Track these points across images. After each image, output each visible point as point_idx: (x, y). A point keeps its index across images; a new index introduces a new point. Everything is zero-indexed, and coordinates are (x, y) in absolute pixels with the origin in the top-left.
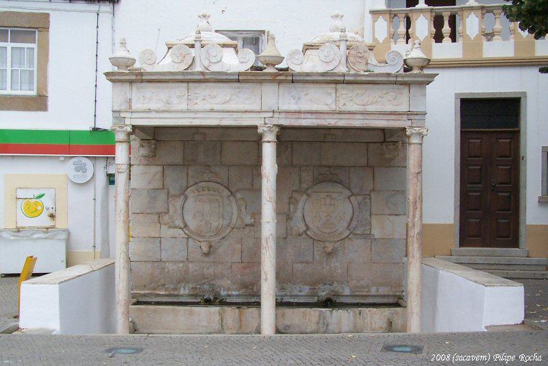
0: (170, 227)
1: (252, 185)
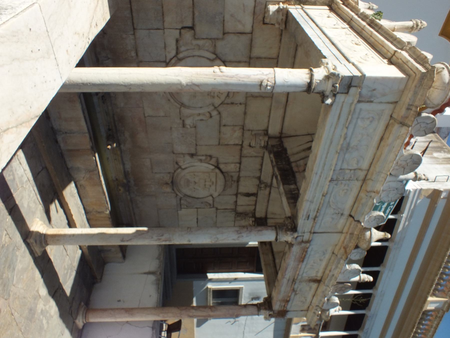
0: (177, 41)
1: (225, 126)
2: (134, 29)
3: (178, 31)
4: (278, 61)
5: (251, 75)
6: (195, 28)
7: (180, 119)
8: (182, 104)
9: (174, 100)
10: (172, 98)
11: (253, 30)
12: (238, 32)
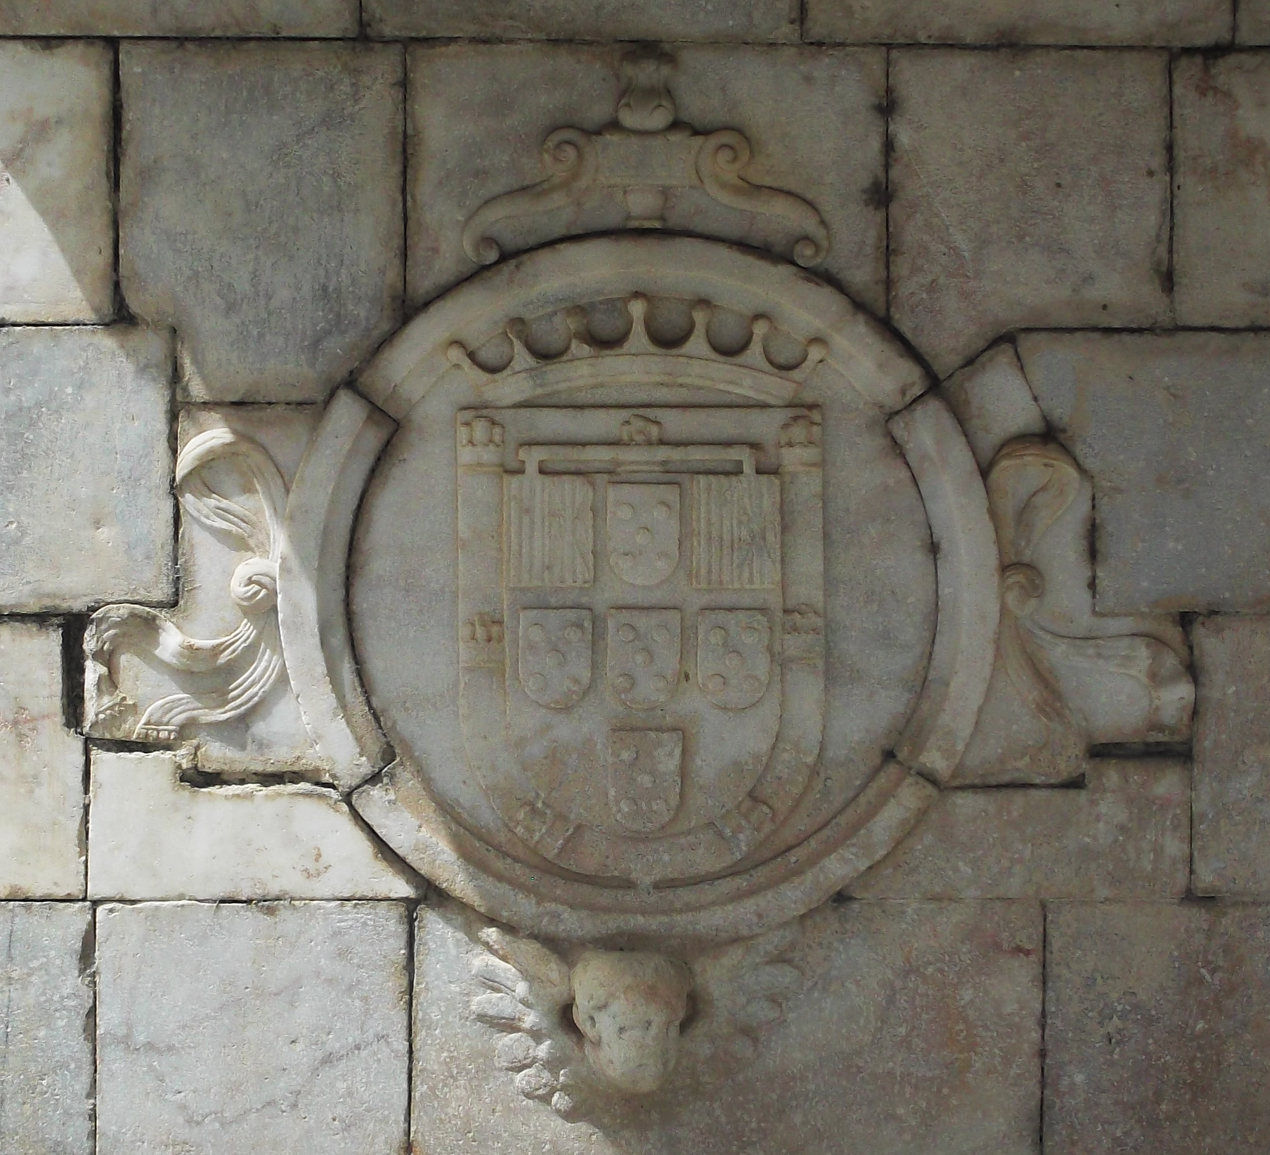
1: (1168, 280)
6: (78, 605)
7: (1075, 784)
9: (831, 847)
10: (815, 859)
11: (89, 39)
12: (104, 186)
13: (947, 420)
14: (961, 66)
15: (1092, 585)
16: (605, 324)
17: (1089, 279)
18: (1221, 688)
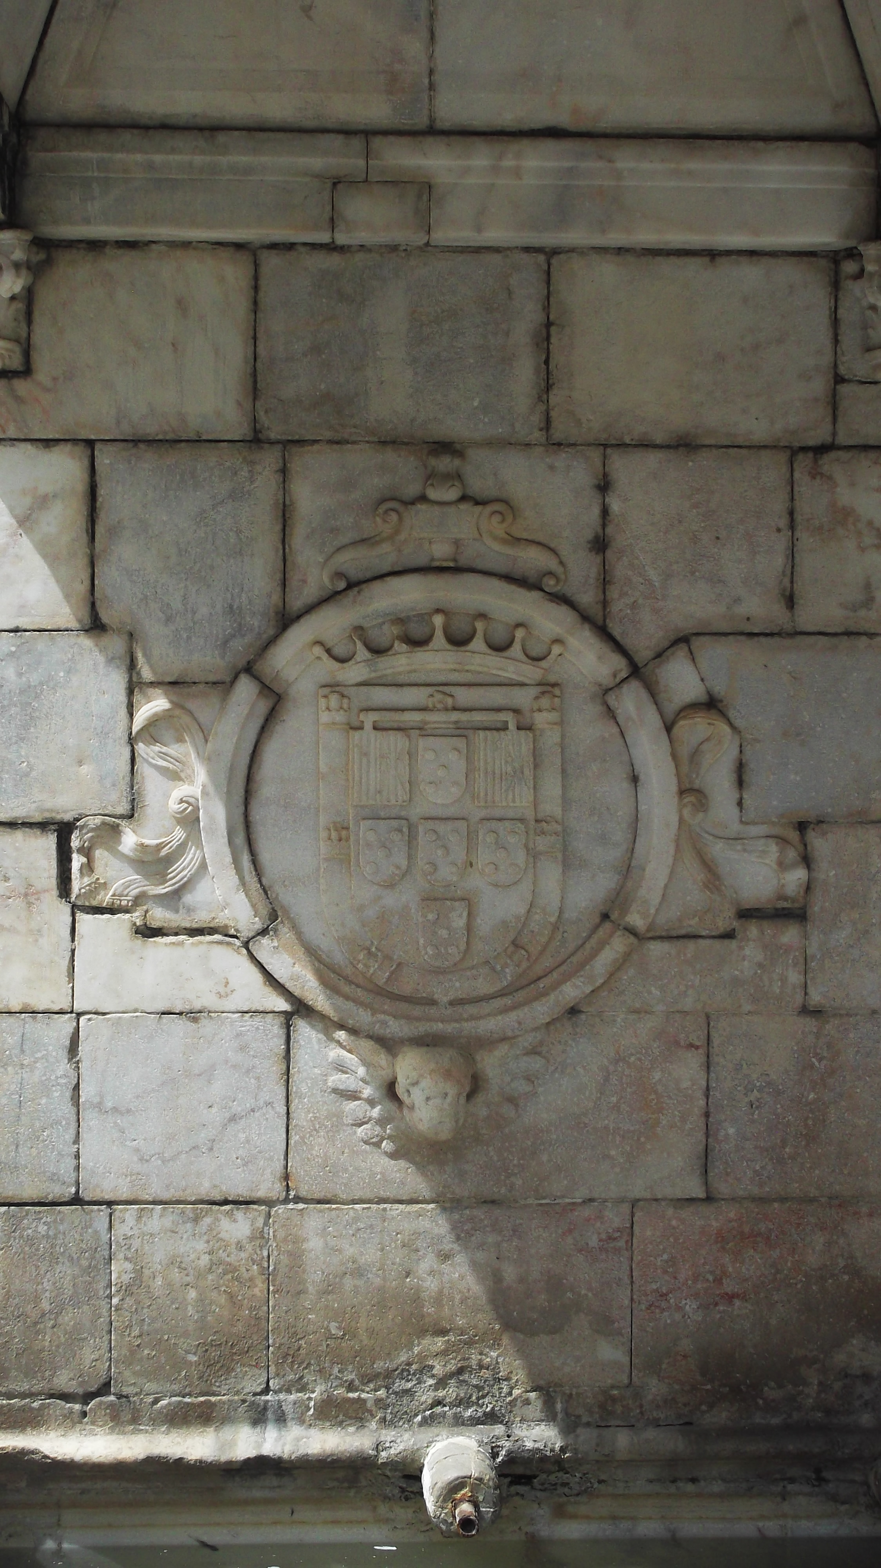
1: (790, 601)
2: (76, 1200)
3: (83, 918)
4: (274, 246)
5: (454, 443)
7: (729, 935)
8: (605, 917)
9: (566, 978)
11: (75, 441)
12: (84, 539)
13: (644, 694)
14: (653, 459)
15: (740, 804)
16: (417, 630)
17: (738, 600)
18: (826, 872)
